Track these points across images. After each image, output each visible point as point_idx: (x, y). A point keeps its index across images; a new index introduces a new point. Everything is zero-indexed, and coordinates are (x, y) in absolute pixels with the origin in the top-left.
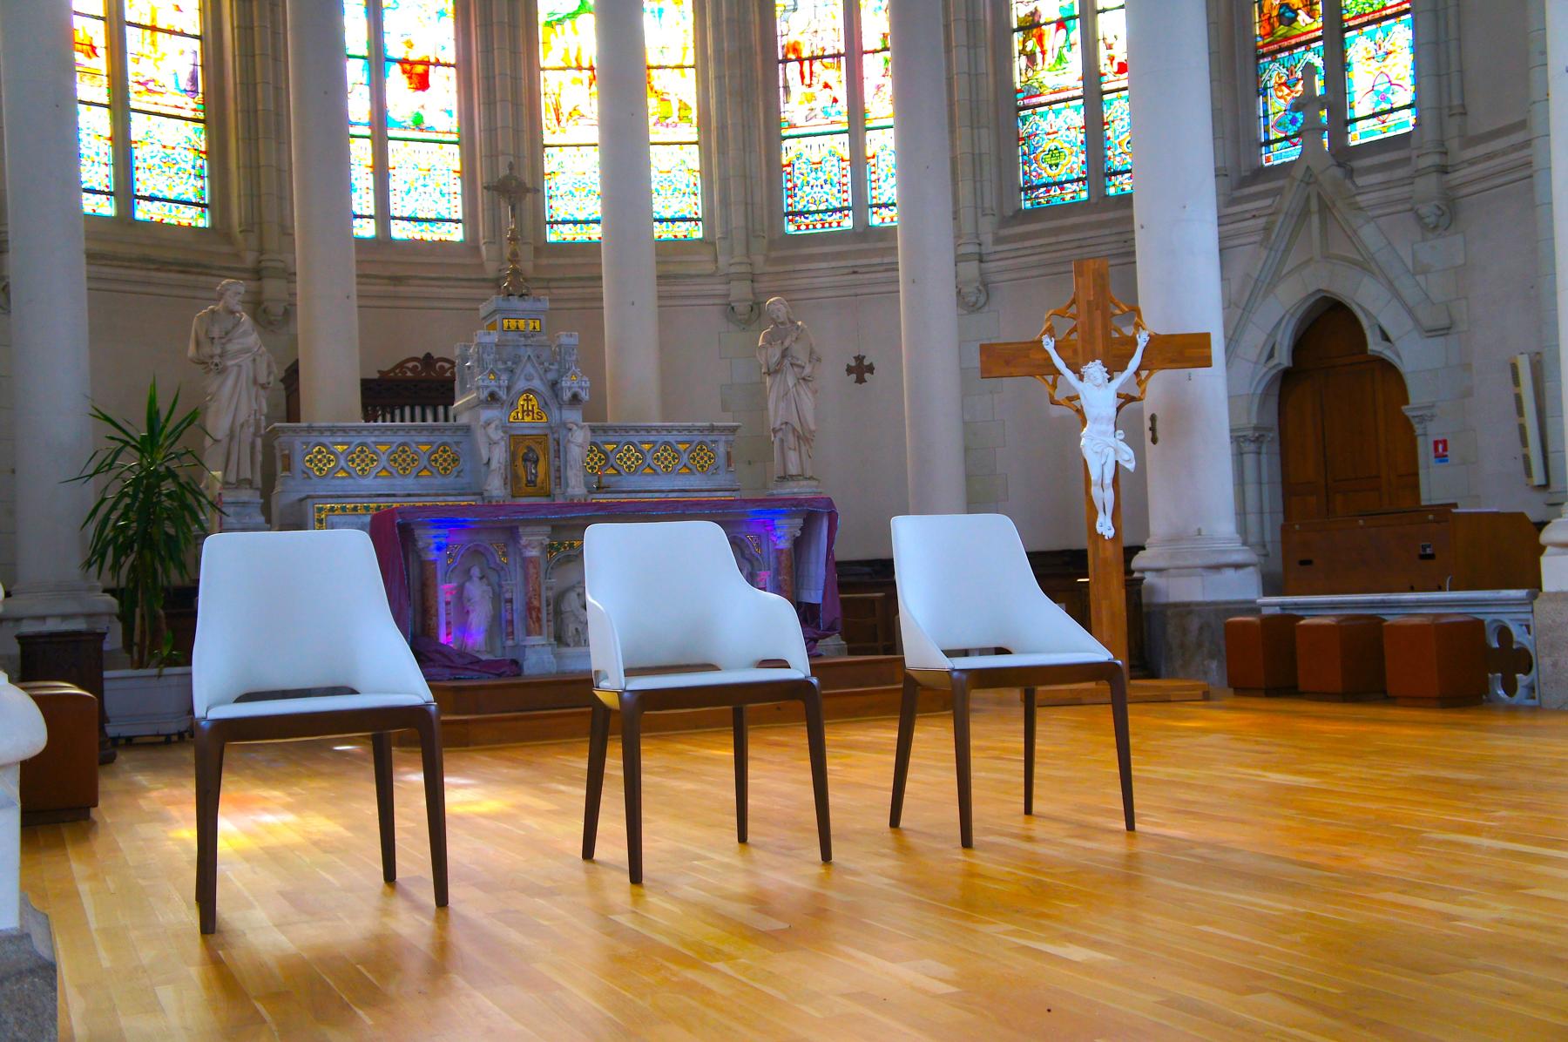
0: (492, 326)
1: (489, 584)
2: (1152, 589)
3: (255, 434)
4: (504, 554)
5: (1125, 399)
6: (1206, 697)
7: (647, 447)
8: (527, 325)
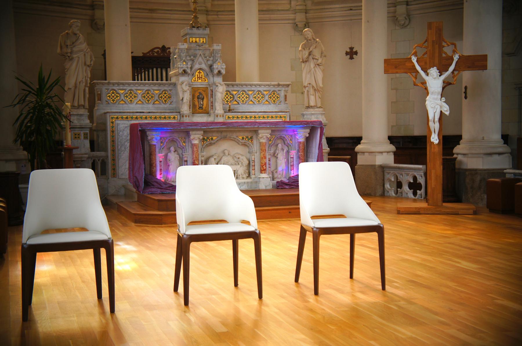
0: (185, 41)
1: (178, 154)
2: (461, 162)
3: (86, 86)
4: (184, 142)
5: (446, 84)
6: (475, 213)
7: (250, 92)
8: (200, 40)
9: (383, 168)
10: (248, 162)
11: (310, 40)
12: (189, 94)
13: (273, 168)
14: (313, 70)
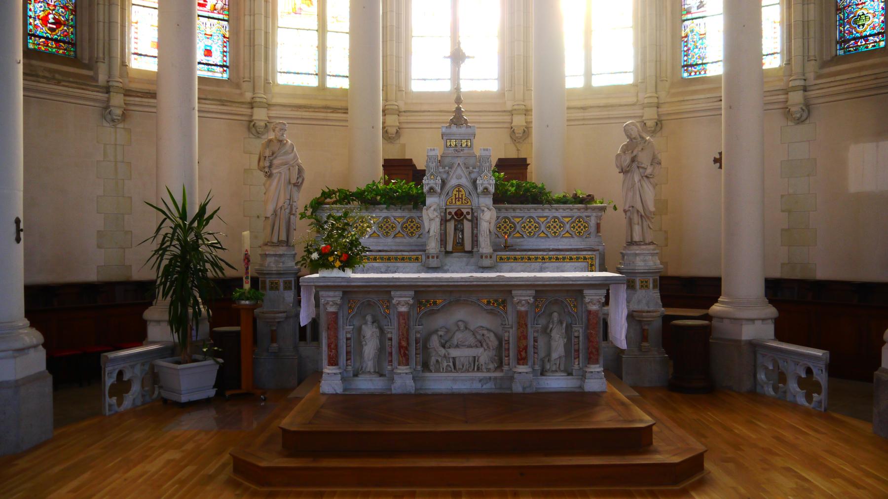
9: (754, 346)
10: (496, 343)
11: (634, 138)
12: (439, 223)
13: (542, 353)
14: (637, 185)
